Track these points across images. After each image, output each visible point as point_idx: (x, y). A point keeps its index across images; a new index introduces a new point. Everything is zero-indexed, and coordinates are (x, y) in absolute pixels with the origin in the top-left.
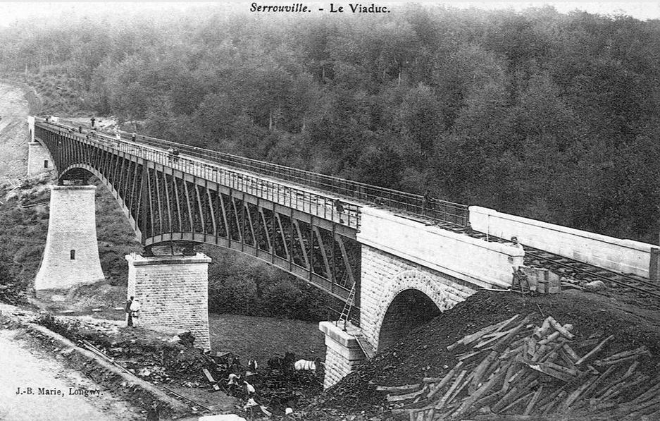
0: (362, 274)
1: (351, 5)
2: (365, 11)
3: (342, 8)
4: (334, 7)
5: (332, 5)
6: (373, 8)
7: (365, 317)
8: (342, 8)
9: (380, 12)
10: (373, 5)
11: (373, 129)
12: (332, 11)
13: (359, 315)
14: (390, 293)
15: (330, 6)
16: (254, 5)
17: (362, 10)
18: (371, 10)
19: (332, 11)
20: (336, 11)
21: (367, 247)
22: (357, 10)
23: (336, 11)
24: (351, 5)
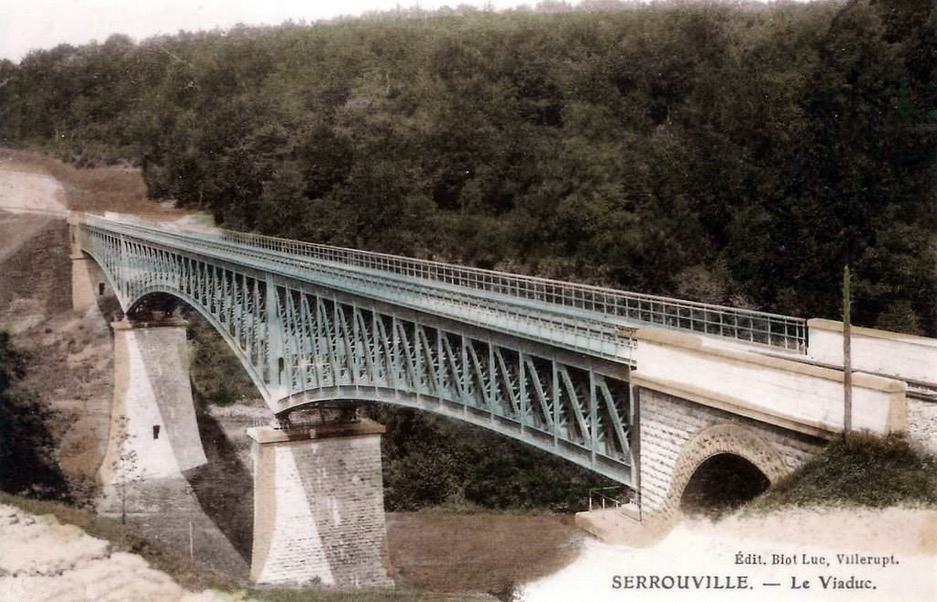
0: (642, 435)
1: (821, 578)
2: (841, 587)
3: (807, 582)
4: (719, 580)
5: (728, 578)
6: (852, 582)
7: (649, 502)
8: (807, 582)
9: (861, 587)
10: (853, 578)
11: (630, 208)
12: (794, 587)
13: (639, 442)
14: (688, 462)
15: (792, 580)
16: (617, 579)
17: (837, 585)
18: (850, 584)
19: (794, 587)
20: (799, 588)
21: (647, 392)
22: (830, 585)
23: (799, 588)
24: (821, 578)
